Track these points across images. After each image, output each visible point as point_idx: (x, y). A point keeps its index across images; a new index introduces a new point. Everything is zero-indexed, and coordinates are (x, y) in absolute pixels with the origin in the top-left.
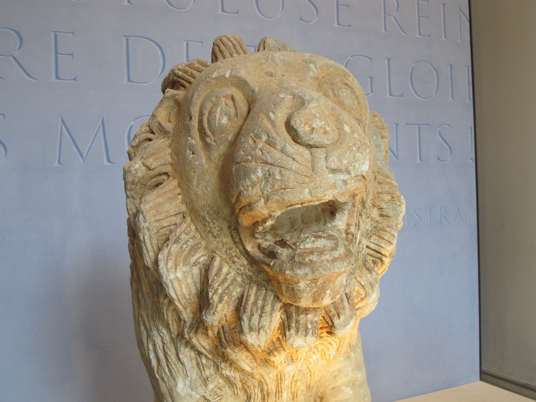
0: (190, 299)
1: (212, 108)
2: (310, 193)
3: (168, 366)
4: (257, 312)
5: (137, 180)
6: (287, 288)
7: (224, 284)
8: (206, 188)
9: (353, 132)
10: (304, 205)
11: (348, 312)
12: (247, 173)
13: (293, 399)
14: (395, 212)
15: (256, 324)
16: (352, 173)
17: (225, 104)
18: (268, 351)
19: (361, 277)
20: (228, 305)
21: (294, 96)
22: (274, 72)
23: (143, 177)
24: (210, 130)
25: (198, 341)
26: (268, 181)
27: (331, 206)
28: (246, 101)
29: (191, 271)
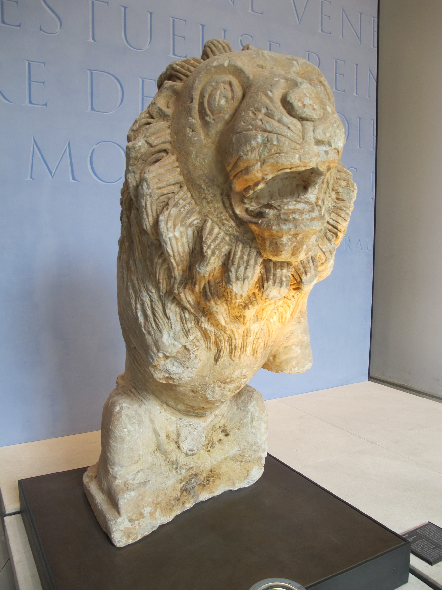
0: (183, 257)
1: (212, 91)
2: (300, 158)
3: (155, 321)
5: (139, 155)
6: (271, 243)
7: (215, 242)
8: (204, 160)
10: (293, 170)
11: (313, 272)
12: (248, 140)
13: (253, 355)
14: (348, 197)
15: (242, 275)
16: (333, 145)
17: (223, 89)
18: (244, 305)
19: (323, 245)
20: (219, 259)
21: (287, 80)
22: (264, 65)
23: (145, 153)
24: (210, 110)
25: (185, 295)
26: (266, 146)
27: (304, 181)
28: (241, 87)
29: (186, 232)
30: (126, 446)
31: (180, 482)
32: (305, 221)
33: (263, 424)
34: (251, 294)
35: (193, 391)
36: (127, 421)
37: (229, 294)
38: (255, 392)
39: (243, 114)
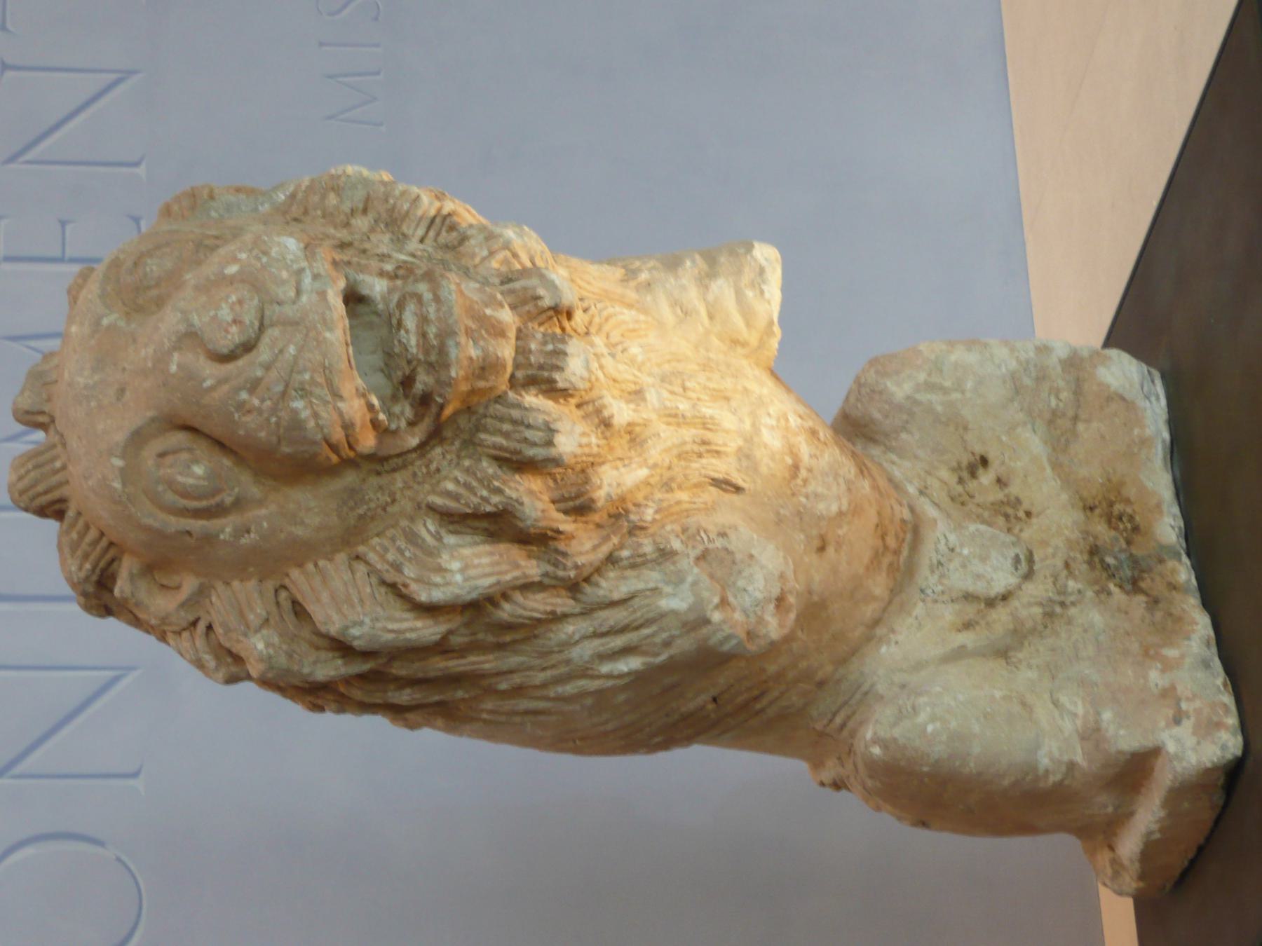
1: (176, 492)
3: (637, 628)
5: (285, 647)
9: (235, 260)
11: (534, 281)
15: (540, 434)
24: (213, 496)
30: (976, 728)
31: (1103, 596)
32: (441, 314)
33: (953, 358)
34: (580, 413)
35: (822, 549)
37: (579, 460)
38: (863, 381)
39: (241, 432)
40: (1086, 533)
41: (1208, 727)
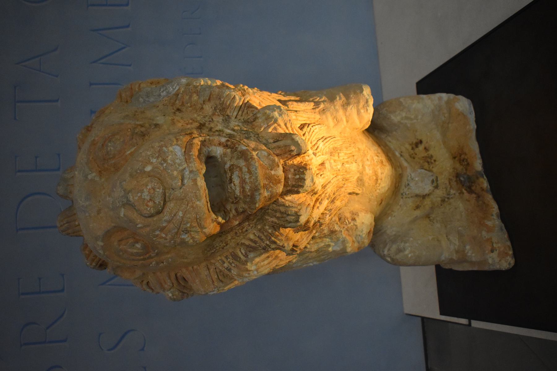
4: (285, 217)
11: (289, 142)
15: (293, 217)
33: (414, 106)
36: (401, 254)
40: (454, 168)
41: (502, 255)
